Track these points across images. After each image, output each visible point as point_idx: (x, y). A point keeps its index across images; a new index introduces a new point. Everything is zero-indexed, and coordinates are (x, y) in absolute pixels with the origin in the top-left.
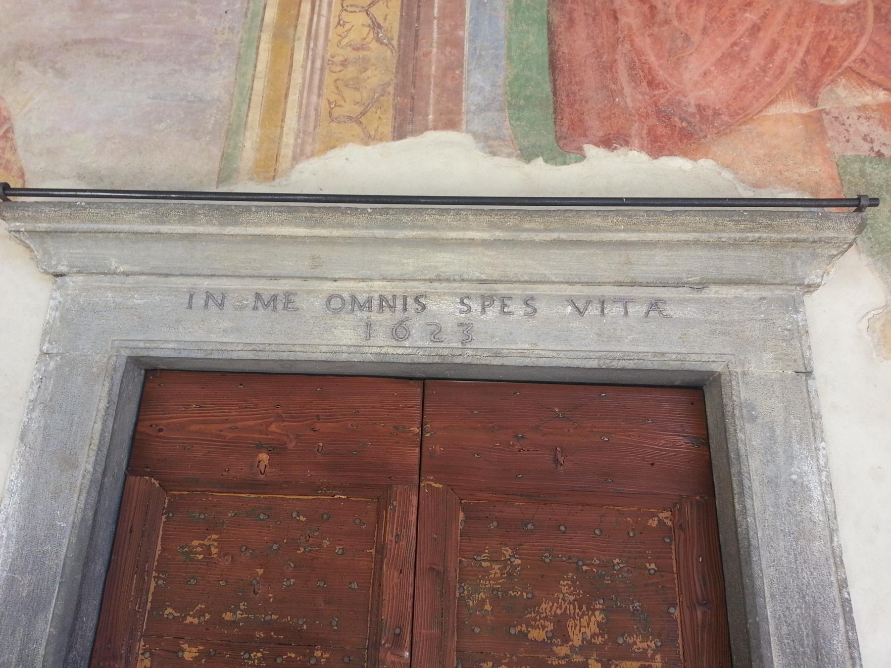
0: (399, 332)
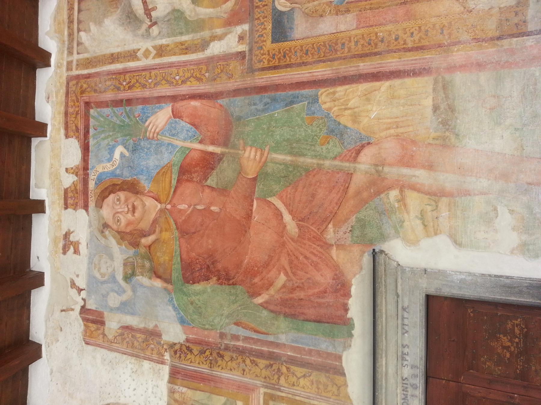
0: (414, 387)
